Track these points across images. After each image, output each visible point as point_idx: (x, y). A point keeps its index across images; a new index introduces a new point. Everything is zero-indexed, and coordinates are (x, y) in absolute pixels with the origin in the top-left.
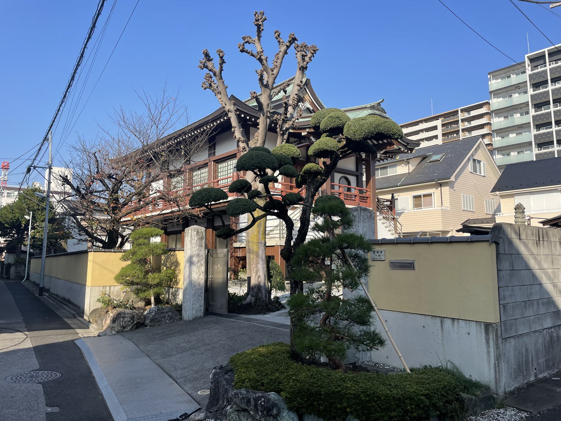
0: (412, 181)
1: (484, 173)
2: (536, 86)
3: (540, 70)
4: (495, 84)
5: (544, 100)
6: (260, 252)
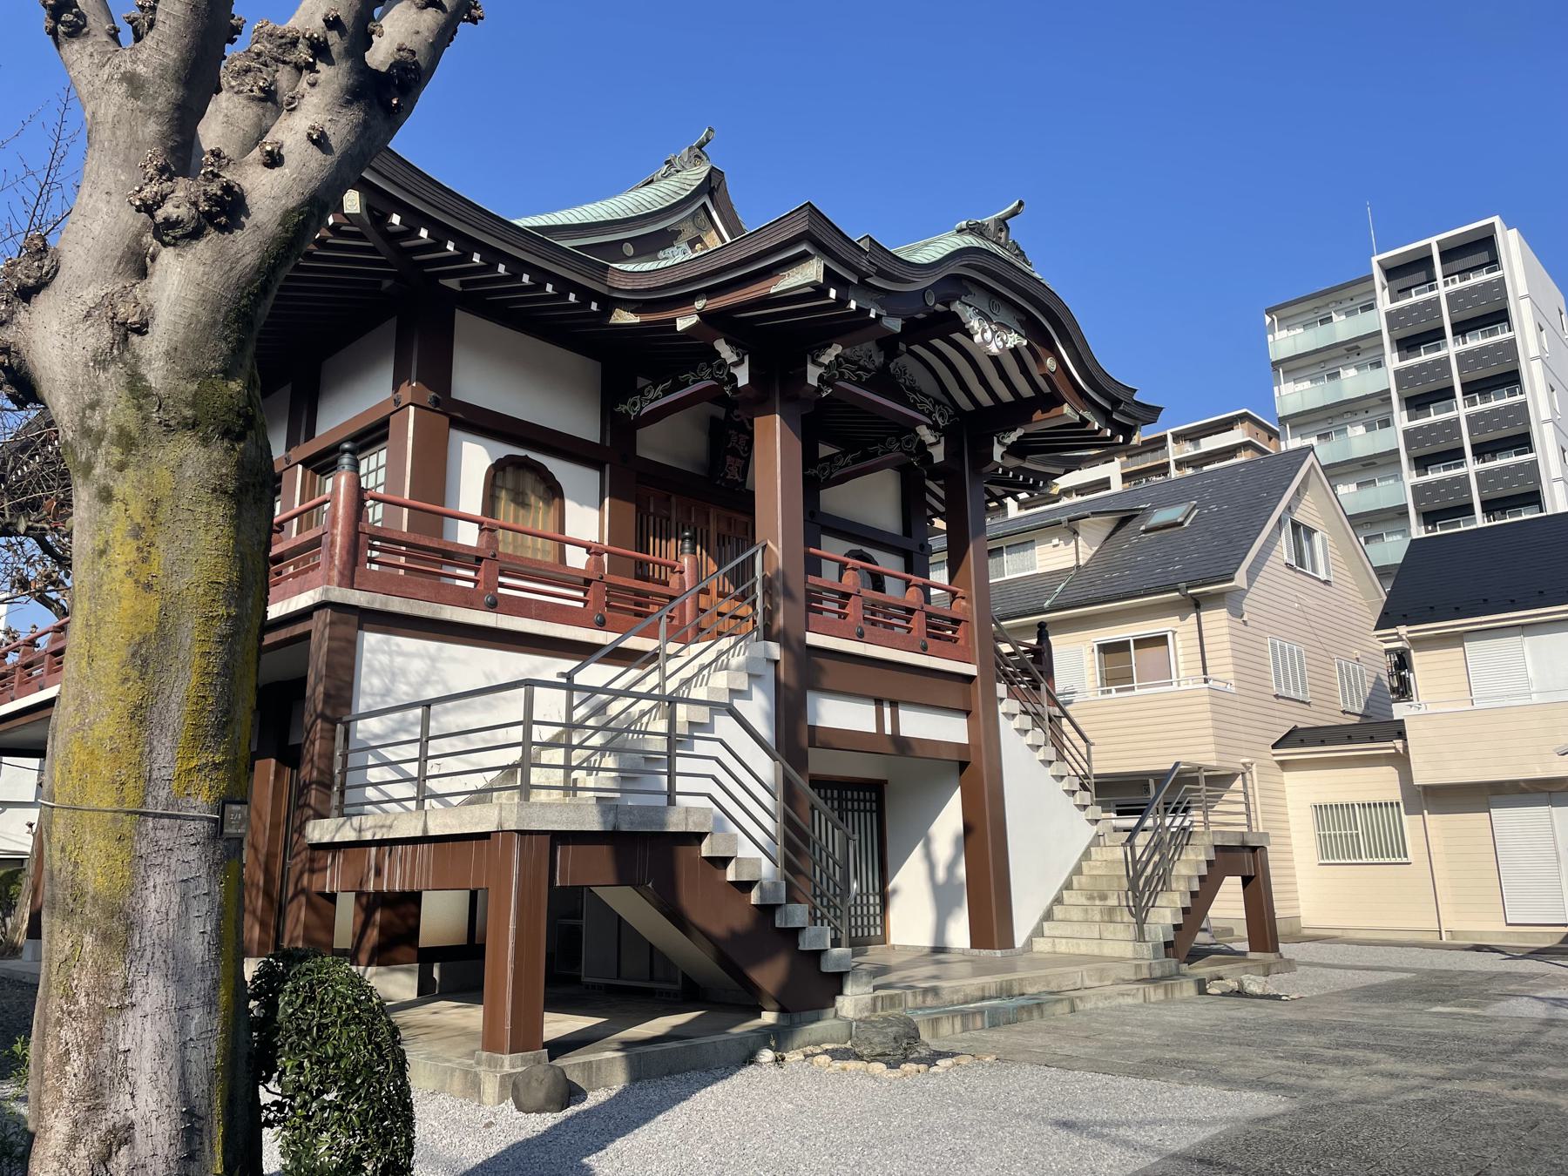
0: (1093, 593)
1: (1328, 572)
2: (1407, 345)
3: (1415, 298)
4: (1286, 341)
5: (1433, 385)
6: (157, 900)
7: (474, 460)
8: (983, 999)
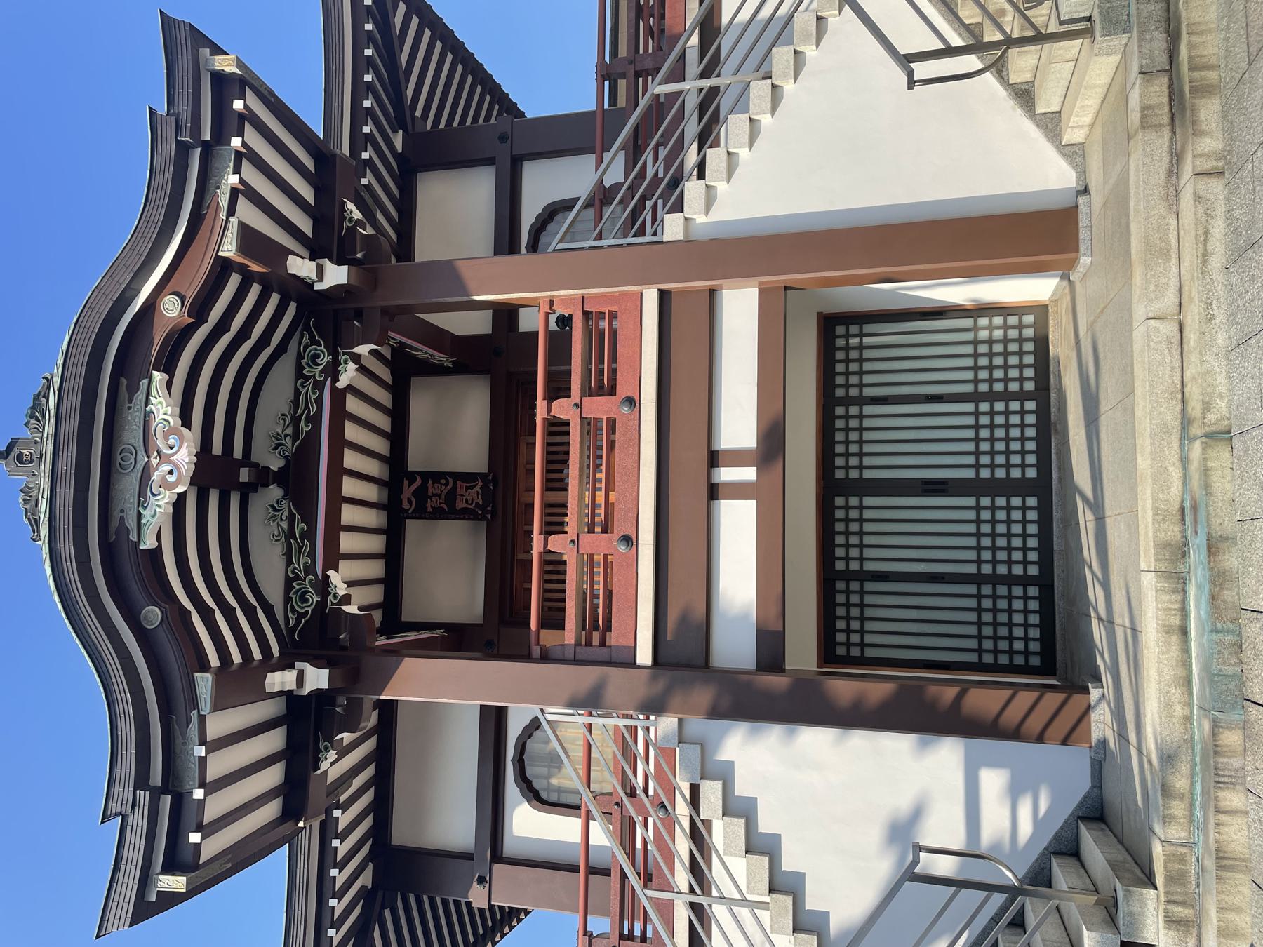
7: (527, 824)
8: (1184, 631)
